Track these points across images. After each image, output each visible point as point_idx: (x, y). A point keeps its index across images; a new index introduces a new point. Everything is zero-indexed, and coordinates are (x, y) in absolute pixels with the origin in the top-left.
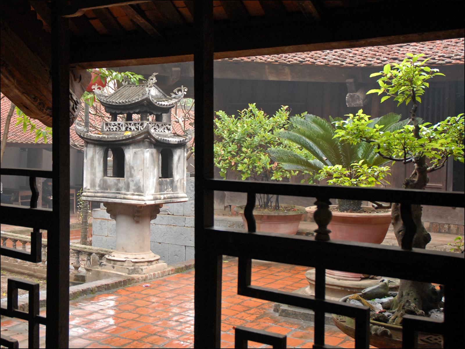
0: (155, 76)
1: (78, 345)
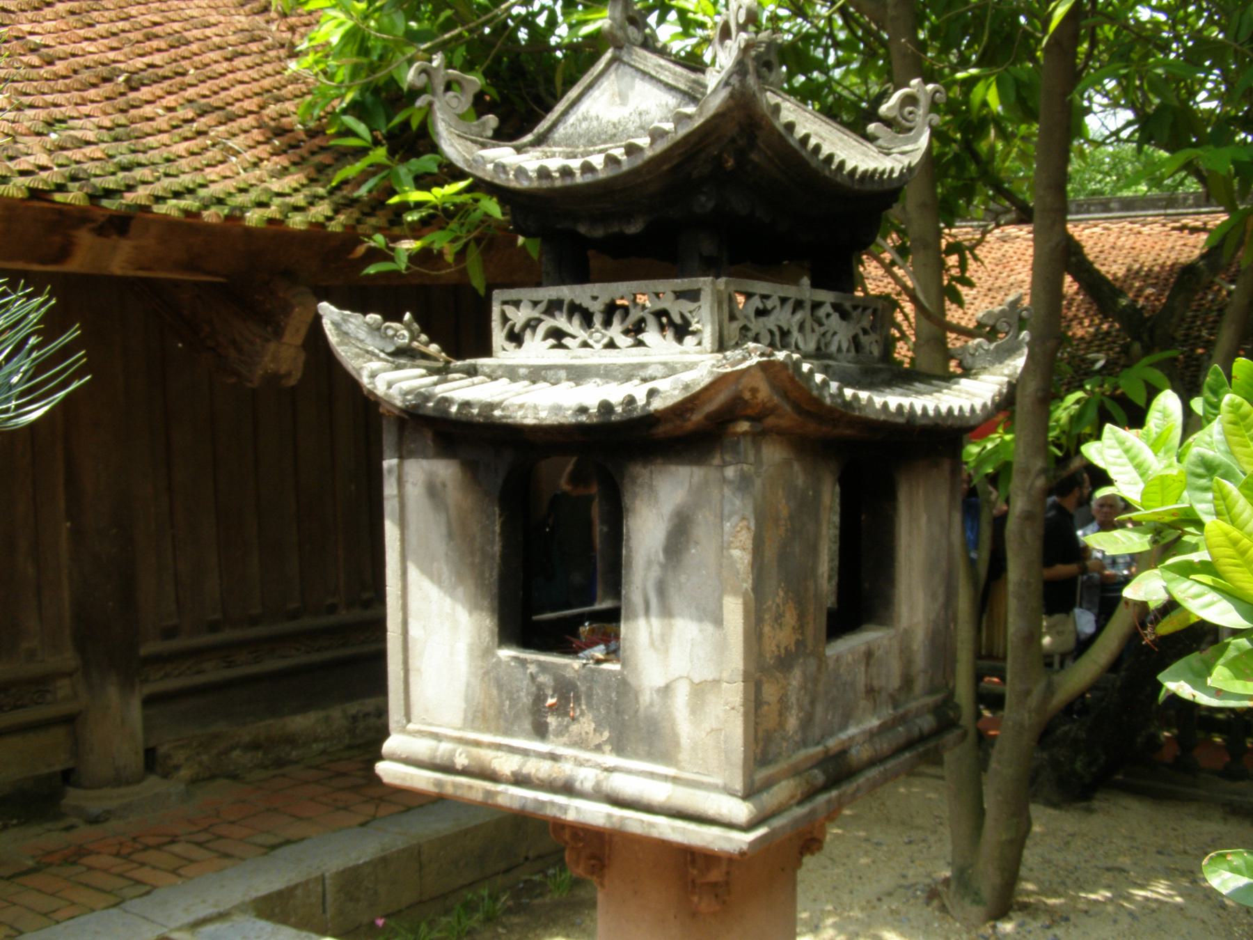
0: (931, 127)
1: (497, 548)
